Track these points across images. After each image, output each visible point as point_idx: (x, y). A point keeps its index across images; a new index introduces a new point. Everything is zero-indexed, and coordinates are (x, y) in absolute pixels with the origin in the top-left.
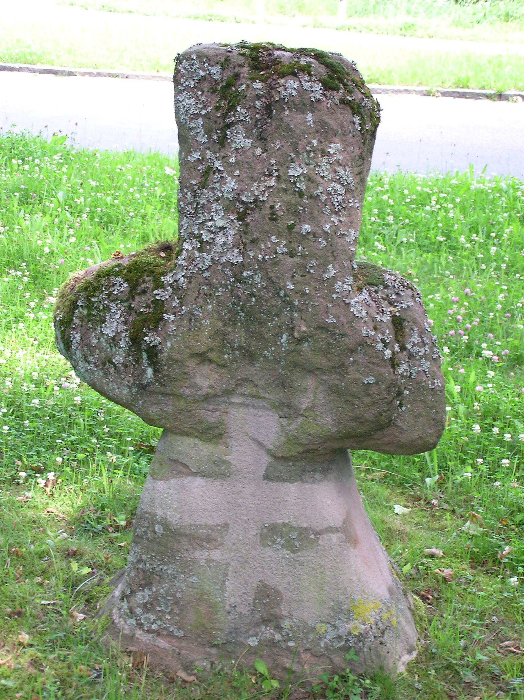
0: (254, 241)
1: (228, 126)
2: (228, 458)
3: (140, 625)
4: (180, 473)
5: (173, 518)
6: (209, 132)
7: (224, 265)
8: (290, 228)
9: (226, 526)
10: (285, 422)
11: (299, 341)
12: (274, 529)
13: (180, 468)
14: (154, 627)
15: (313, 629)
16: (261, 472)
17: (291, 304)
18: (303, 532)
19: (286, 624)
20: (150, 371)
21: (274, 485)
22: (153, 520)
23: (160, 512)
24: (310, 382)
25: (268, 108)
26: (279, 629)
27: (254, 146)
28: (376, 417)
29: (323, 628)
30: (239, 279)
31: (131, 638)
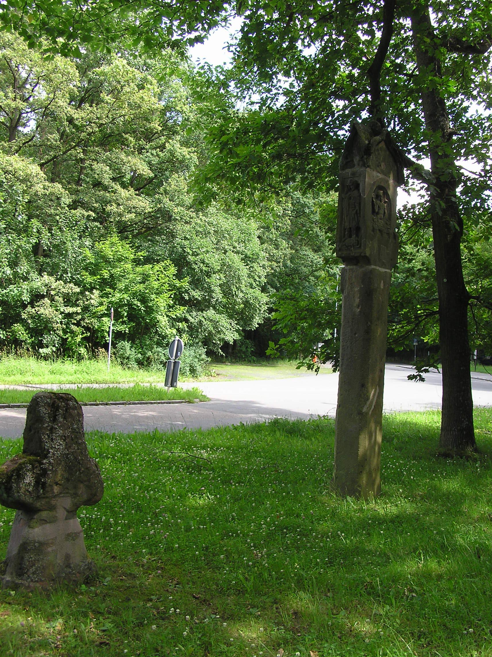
0: (70, 447)
1: (57, 415)
2: (57, 515)
3: (32, 581)
4: (43, 524)
5: (41, 539)
6: (49, 417)
7: (64, 454)
8: (77, 442)
9: (56, 537)
10: (73, 499)
11: (81, 473)
12: (69, 535)
13: (43, 522)
14: (36, 579)
15: (79, 565)
16: (64, 518)
17: (79, 463)
18: (76, 533)
19: (72, 566)
20: (42, 490)
21: (67, 521)
22: (35, 542)
23: (37, 539)
24: (82, 485)
25: (66, 410)
26: (70, 567)
27: (63, 421)
28: (300, 430)
29: (81, 564)
30: (67, 458)
31: (29, 587)
